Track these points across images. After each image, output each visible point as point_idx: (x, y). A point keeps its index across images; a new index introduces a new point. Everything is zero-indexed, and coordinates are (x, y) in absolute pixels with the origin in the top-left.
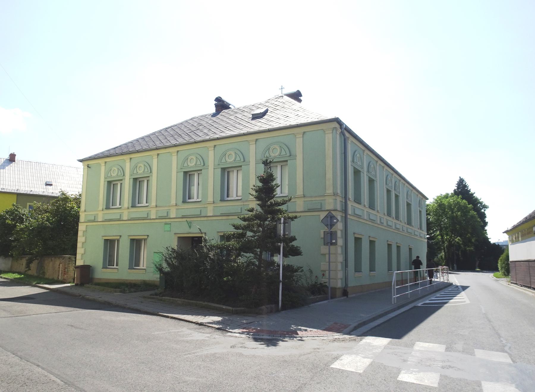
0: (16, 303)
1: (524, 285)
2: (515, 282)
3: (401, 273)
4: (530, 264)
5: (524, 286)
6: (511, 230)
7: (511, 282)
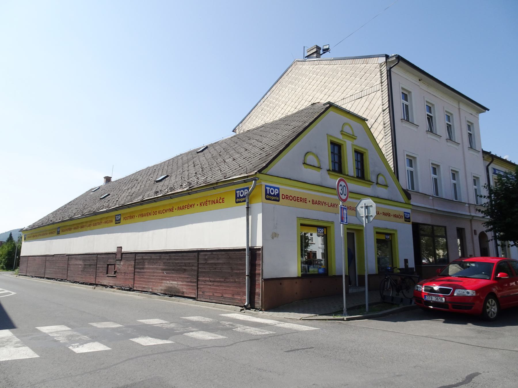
0: (382, 239)
1: (36, 276)
2: (25, 274)
3: (108, 274)
4: (47, 258)
5: (35, 277)
6: (27, 230)
7: (20, 274)
